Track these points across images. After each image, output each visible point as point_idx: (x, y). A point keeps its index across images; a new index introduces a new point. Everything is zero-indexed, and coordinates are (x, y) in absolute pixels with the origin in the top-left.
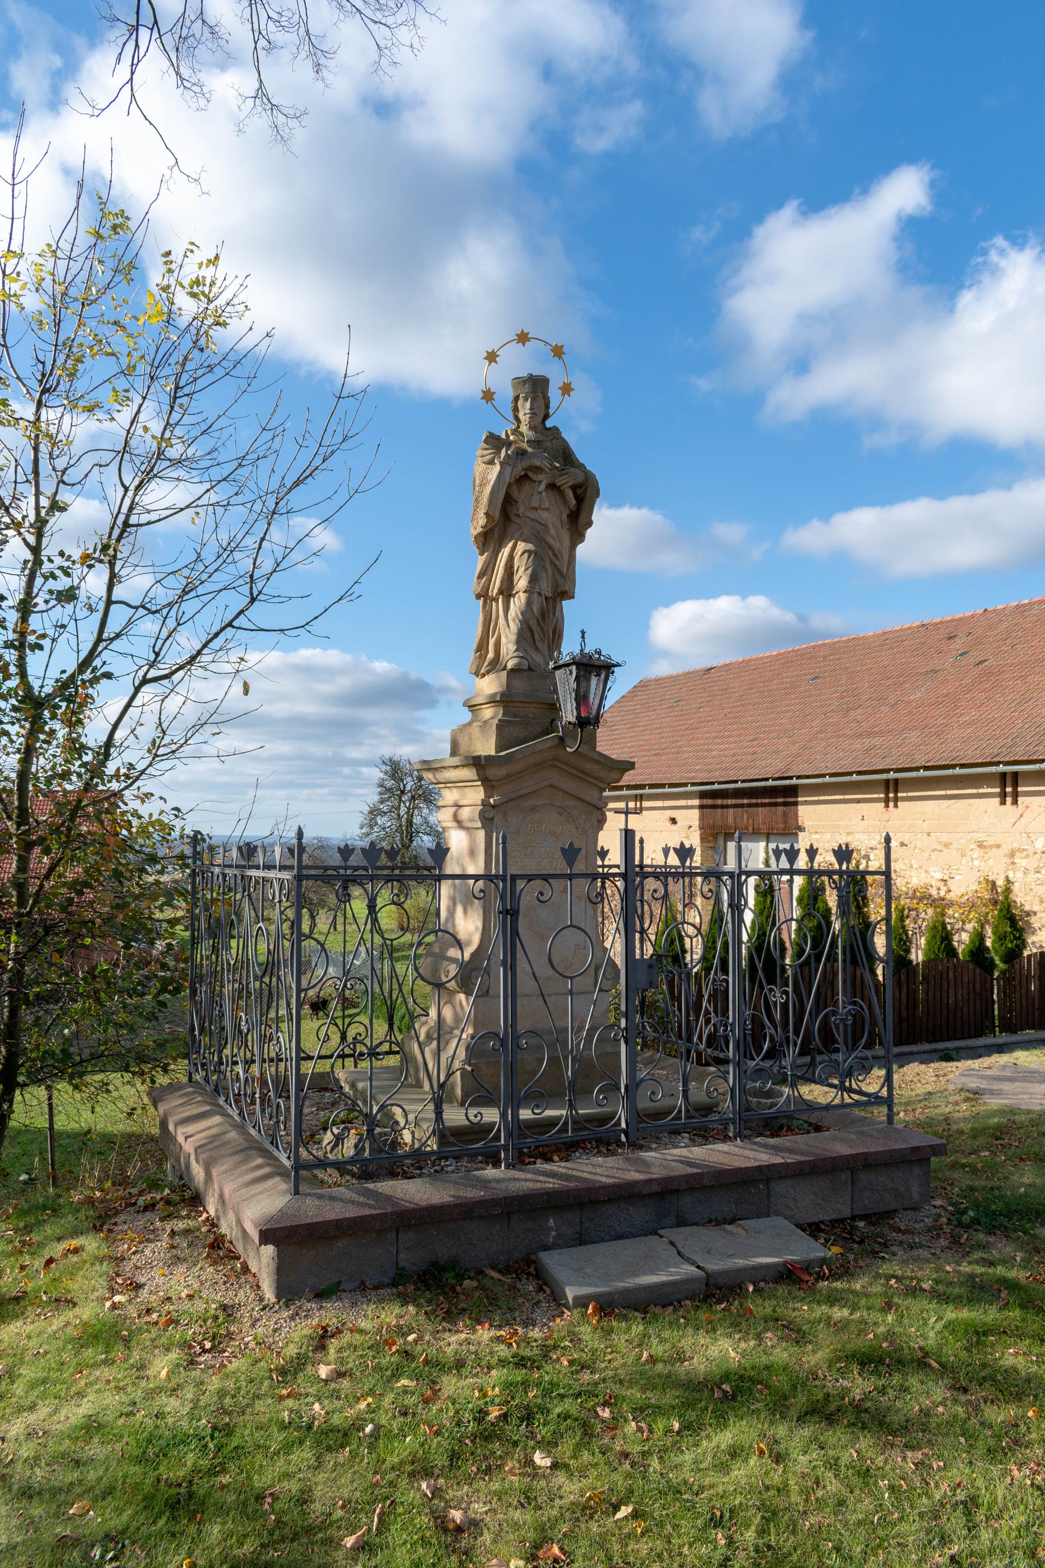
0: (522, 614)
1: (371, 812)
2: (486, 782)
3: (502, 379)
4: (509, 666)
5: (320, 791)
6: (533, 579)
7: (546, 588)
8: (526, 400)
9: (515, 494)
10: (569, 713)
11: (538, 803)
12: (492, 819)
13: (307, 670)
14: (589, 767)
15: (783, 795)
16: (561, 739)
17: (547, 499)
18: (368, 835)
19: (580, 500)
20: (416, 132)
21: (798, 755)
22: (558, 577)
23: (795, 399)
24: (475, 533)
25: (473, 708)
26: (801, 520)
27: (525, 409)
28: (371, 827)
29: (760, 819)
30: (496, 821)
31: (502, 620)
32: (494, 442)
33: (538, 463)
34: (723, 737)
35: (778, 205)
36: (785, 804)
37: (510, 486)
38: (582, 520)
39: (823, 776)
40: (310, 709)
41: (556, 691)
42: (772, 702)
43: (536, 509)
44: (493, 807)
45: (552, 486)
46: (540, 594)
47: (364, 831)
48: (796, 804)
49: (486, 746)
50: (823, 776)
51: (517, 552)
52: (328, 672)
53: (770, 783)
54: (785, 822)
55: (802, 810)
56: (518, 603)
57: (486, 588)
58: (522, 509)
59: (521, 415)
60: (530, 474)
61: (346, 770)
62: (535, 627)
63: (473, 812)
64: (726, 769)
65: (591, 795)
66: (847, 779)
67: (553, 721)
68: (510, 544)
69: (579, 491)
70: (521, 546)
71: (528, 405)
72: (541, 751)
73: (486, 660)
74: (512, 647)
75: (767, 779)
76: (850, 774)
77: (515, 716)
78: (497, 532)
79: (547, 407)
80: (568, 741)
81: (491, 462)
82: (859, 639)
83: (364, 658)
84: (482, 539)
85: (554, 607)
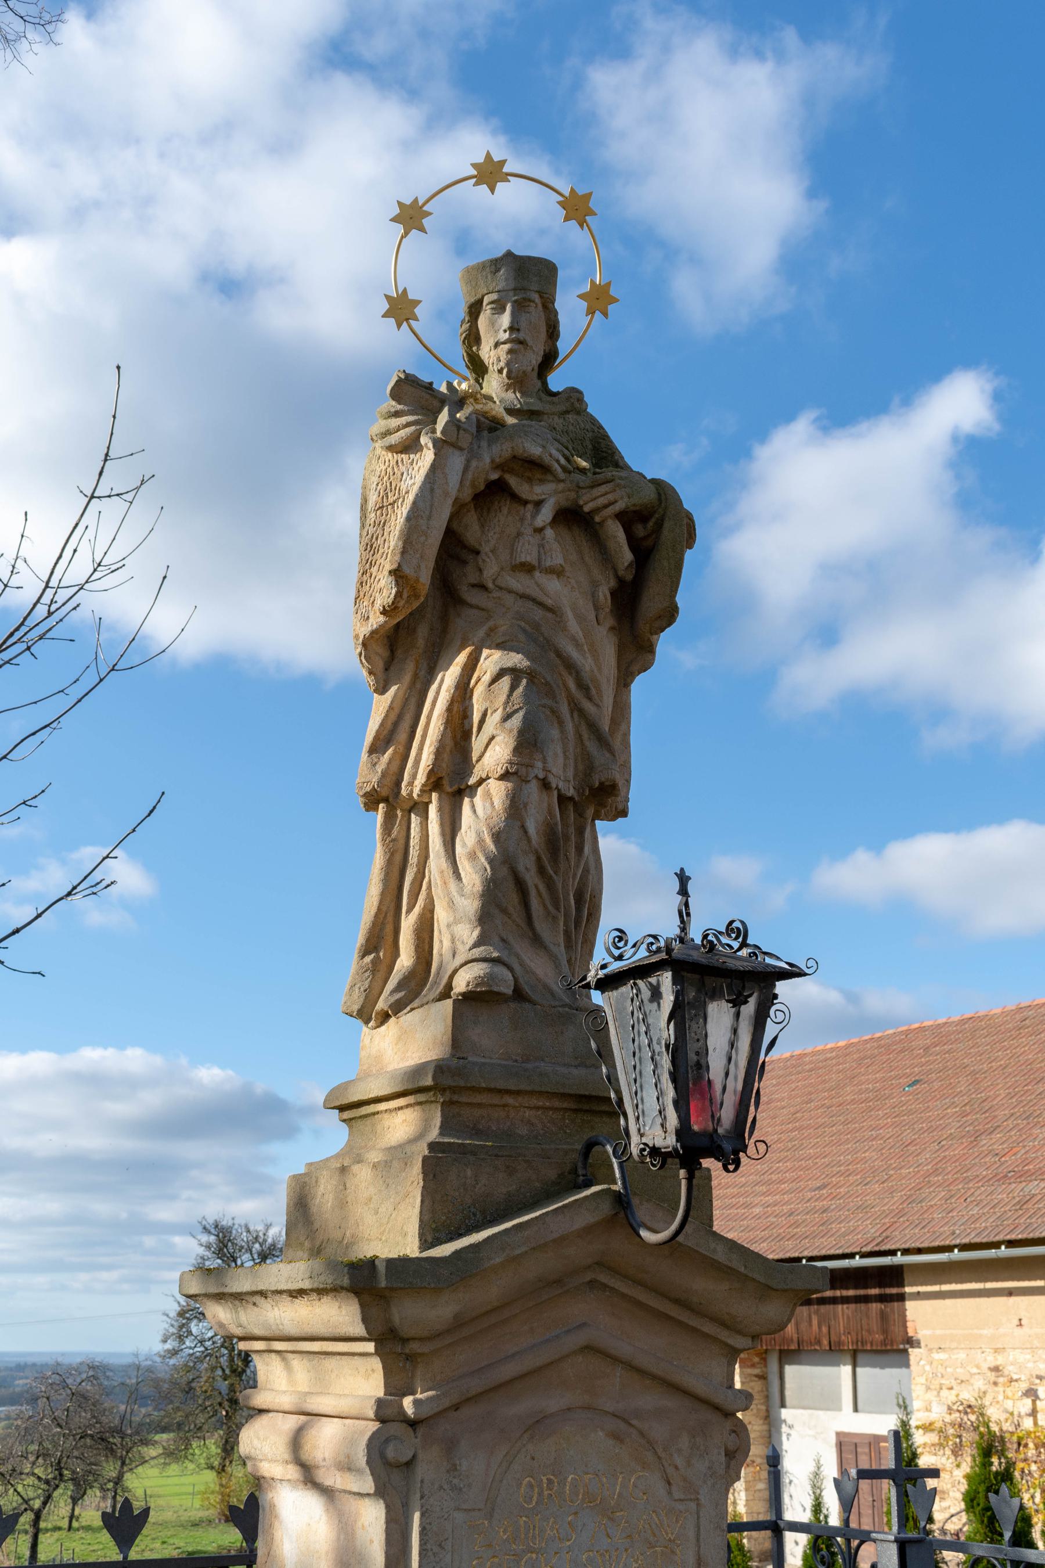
0: (497, 837)
1: (181, 1314)
2: (392, 1344)
3: (436, 275)
4: (460, 984)
5: (105, 1275)
6: (527, 743)
7: (559, 765)
8: (499, 308)
9: (472, 530)
10: (651, 1121)
11: (553, 1403)
12: (410, 1464)
13: (96, 1082)
14: (703, 1287)
15: (879, 1283)
16: (621, 1202)
17: (558, 548)
18: (174, 1353)
19: (643, 554)
20: (275, 317)
21: (901, 1213)
22: (592, 746)
23: (819, 680)
24: (365, 630)
25: (352, 1109)
26: (841, 852)
27: (496, 330)
28: (181, 1339)
29: (841, 1325)
30: (421, 1470)
31: (437, 862)
32: (415, 395)
33: (535, 450)
34: (769, 1183)
35: (789, 417)
36: (882, 1299)
37: (456, 515)
38: (650, 604)
39: (949, 1249)
40: (93, 1142)
41: (605, 1053)
42: (846, 1123)
43: (527, 568)
44: (413, 1424)
45: (571, 517)
46: (545, 785)
47: (169, 1346)
48: (901, 1298)
49: (390, 1225)
50: (949, 1249)
51: (483, 679)
52: (130, 1084)
53: (858, 1262)
54: (885, 1331)
55: (913, 1309)
56: (483, 810)
57: (395, 777)
58: (491, 570)
59: (487, 353)
60: (512, 481)
61: (149, 1241)
62: (532, 879)
63: (350, 1441)
64: (780, 1238)
65: (697, 1371)
66: (992, 1253)
67: (590, 1145)
68: (461, 658)
69: (640, 531)
70: (491, 661)
71: (505, 319)
72: (561, 1241)
73: (390, 981)
74: (468, 933)
75: (851, 1256)
76: (996, 1245)
77: (477, 1132)
78: (423, 632)
79: (553, 331)
80: (642, 1210)
81: (410, 446)
82: (980, 1019)
83: (184, 1061)
84: (381, 651)
85: (580, 832)
